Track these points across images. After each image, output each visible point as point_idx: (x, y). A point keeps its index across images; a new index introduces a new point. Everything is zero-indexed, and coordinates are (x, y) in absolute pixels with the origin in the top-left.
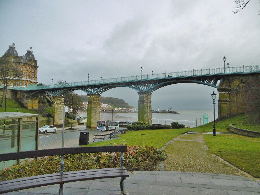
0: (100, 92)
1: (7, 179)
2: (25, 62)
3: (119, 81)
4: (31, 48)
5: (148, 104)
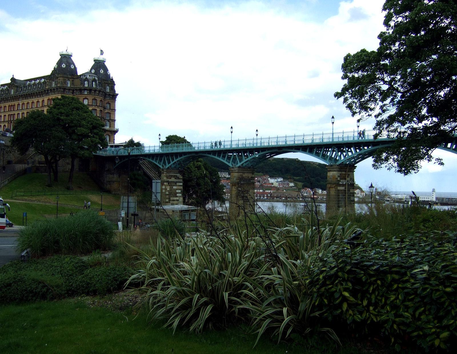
0: (358, 158)
1: (383, 158)
2: (93, 86)
3: (290, 143)
4: (102, 53)
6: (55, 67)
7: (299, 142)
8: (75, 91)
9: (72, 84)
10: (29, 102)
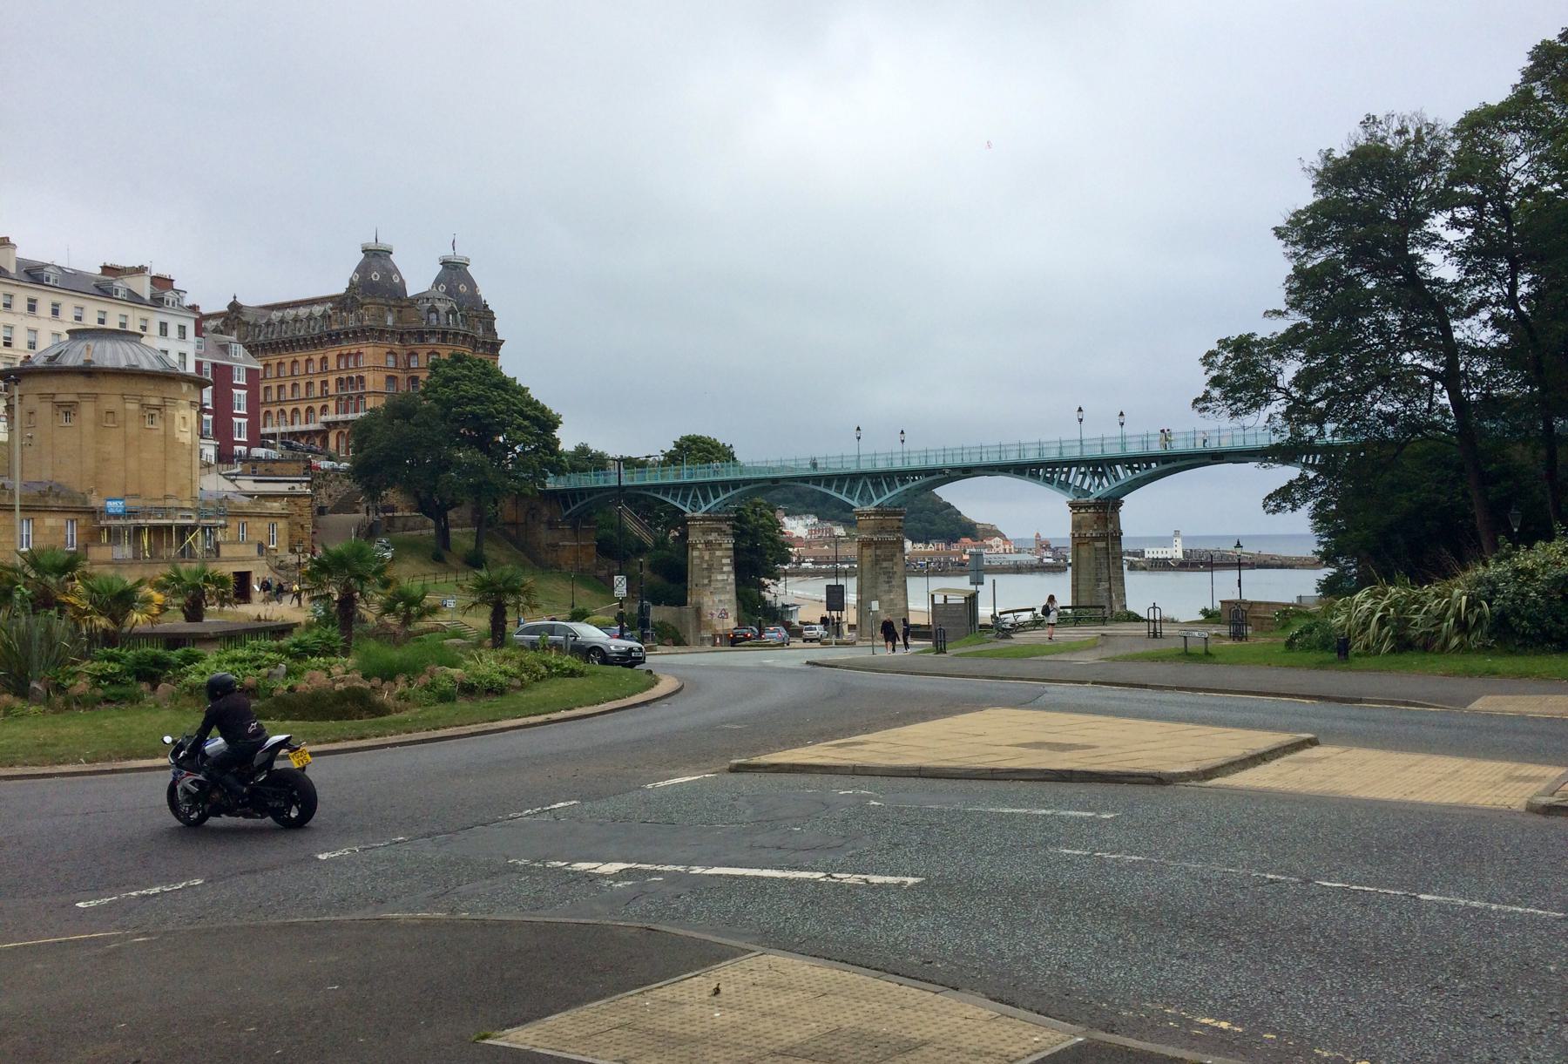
5: (1107, 544)
6: (351, 279)
7: (993, 459)
8: (406, 337)
9: (399, 319)
10: (284, 360)
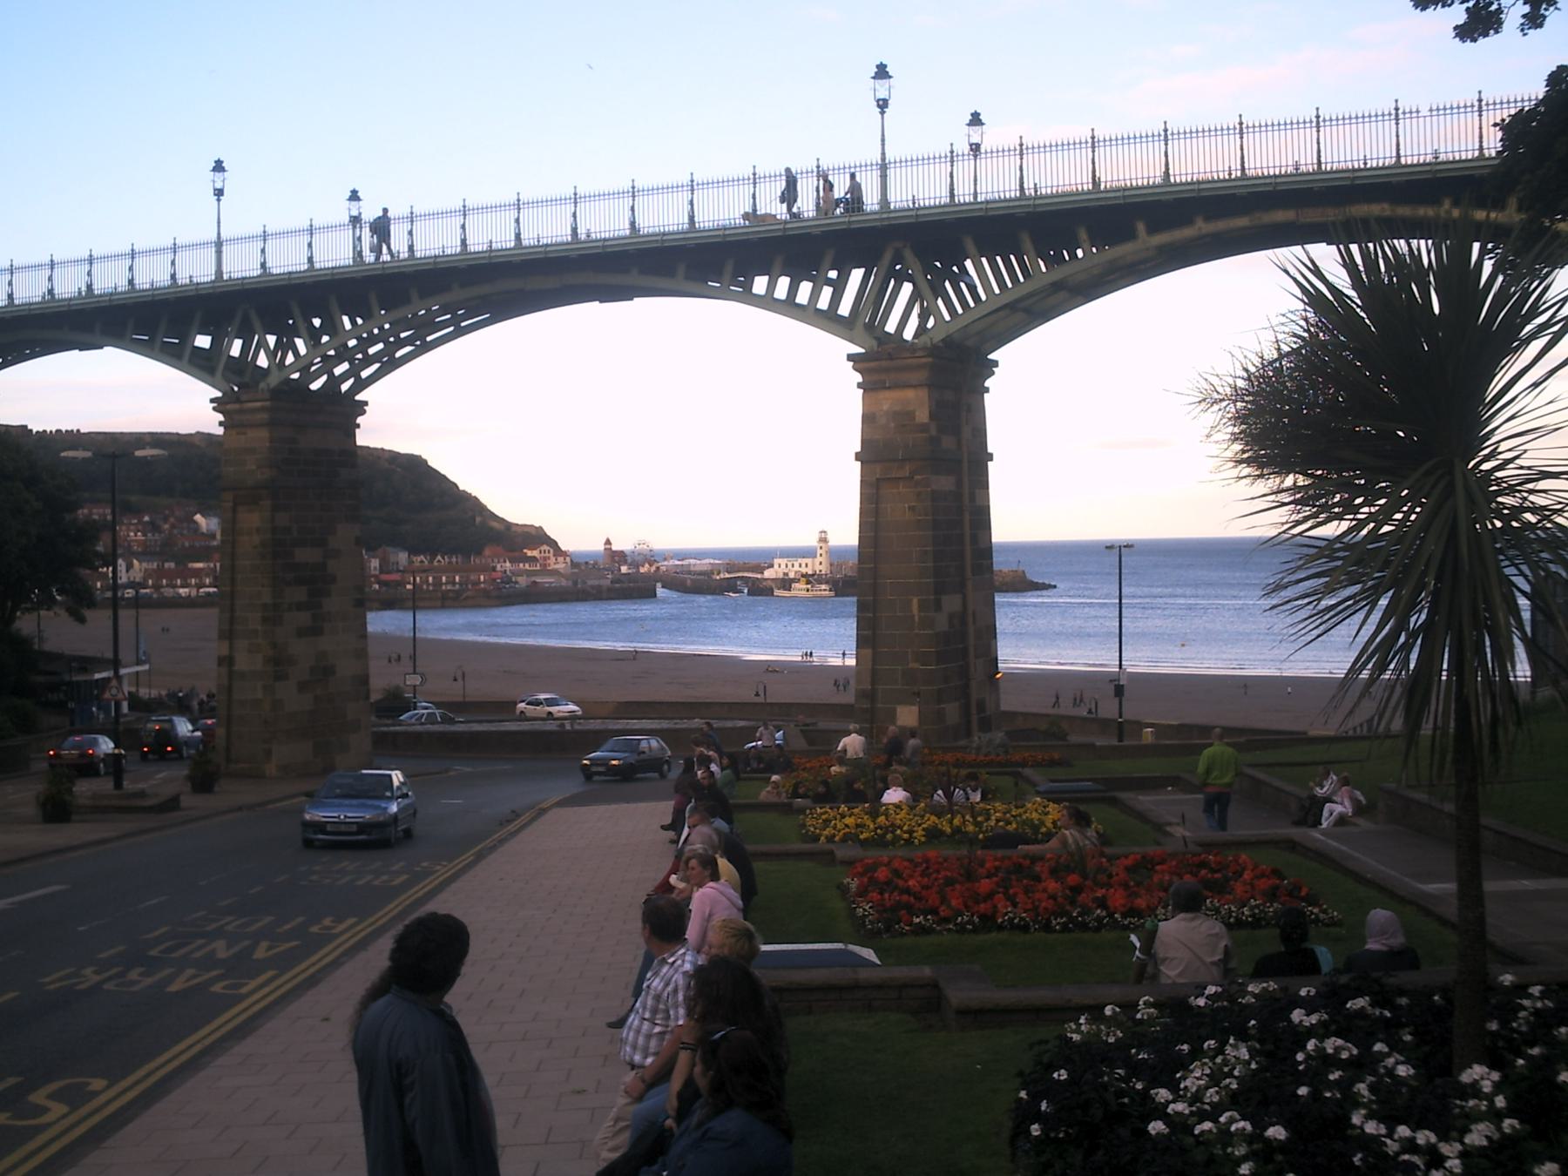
0: (368, 361)
5: (959, 483)
